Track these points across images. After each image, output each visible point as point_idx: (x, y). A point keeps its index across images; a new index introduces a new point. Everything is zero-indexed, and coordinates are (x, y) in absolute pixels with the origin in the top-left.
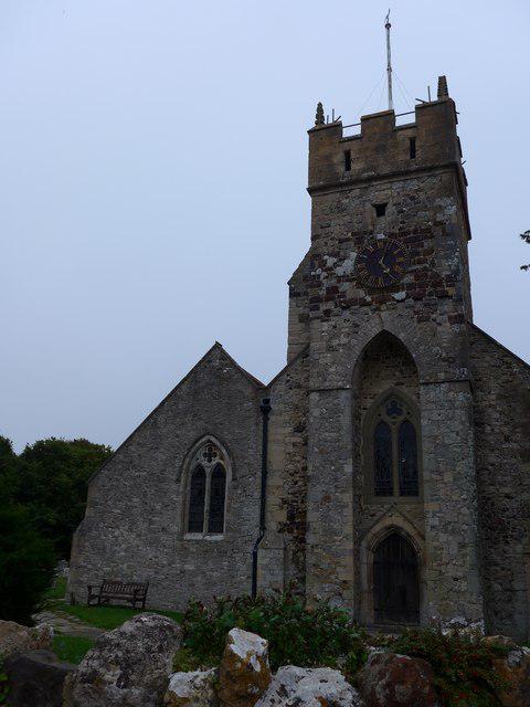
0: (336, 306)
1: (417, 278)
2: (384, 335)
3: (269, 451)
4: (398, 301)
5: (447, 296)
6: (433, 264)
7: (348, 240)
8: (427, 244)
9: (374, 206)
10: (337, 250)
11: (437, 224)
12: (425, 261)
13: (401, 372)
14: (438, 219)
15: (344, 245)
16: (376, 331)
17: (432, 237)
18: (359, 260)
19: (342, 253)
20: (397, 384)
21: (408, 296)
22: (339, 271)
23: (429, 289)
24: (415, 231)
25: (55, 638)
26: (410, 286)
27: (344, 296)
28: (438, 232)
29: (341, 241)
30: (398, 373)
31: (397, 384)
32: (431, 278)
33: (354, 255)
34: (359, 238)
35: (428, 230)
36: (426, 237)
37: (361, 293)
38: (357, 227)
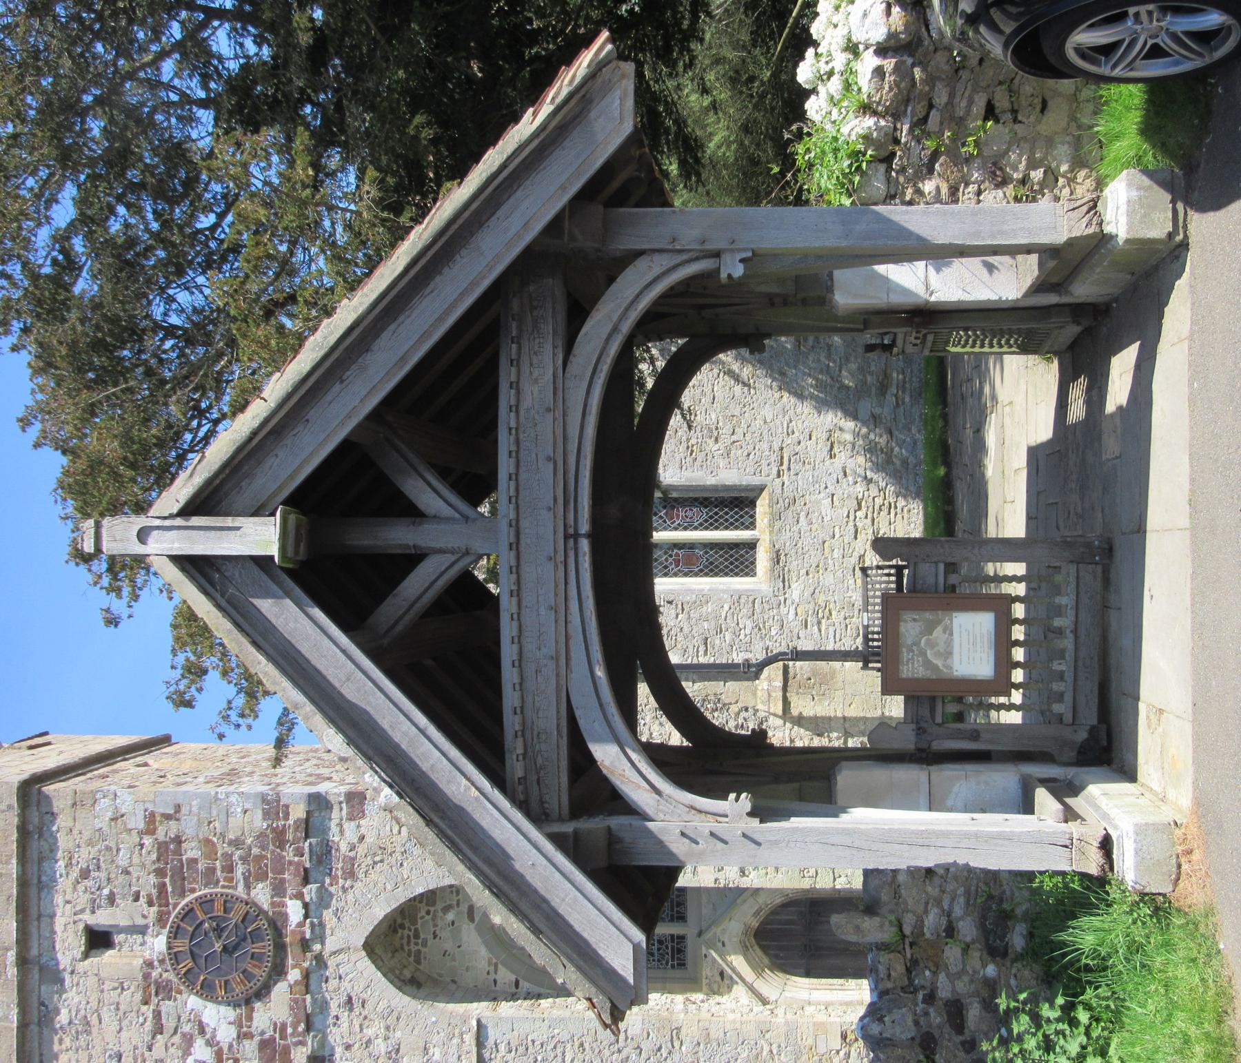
0: (303, 1043)
1: (262, 877)
2: (370, 947)
3: (313, 414)
4: (306, 916)
5: (307, 821)
6: (237, 843)
7: (157, 1015)
8: (191, 851)
9: (86, 955)
10: (177, 1039)
11: (150, 829)
12: (228, 857)
13: (447, 909)
14: (142, 825)
15: (169, 1023)
16: (366, 966)
17: (178, 840)
18: (207, 991)
19: (187, 1028)
20: (471, 919)
21: (299, 896)
22: (226, 1034)
23: (289, 854)
24: (160, 873)
25: (643, 50)
26: (279, 889)
27: (284, 1027)
28: (164, 831)
29: (158, 1029)
30: (450, 916)
31: (471, 919)
32: (263, 848)
33: (193, 1001)
34: (155, 990)
35: (162, 847)
36: (178, 852)
37: (280, 991)
38: (132, 996)
